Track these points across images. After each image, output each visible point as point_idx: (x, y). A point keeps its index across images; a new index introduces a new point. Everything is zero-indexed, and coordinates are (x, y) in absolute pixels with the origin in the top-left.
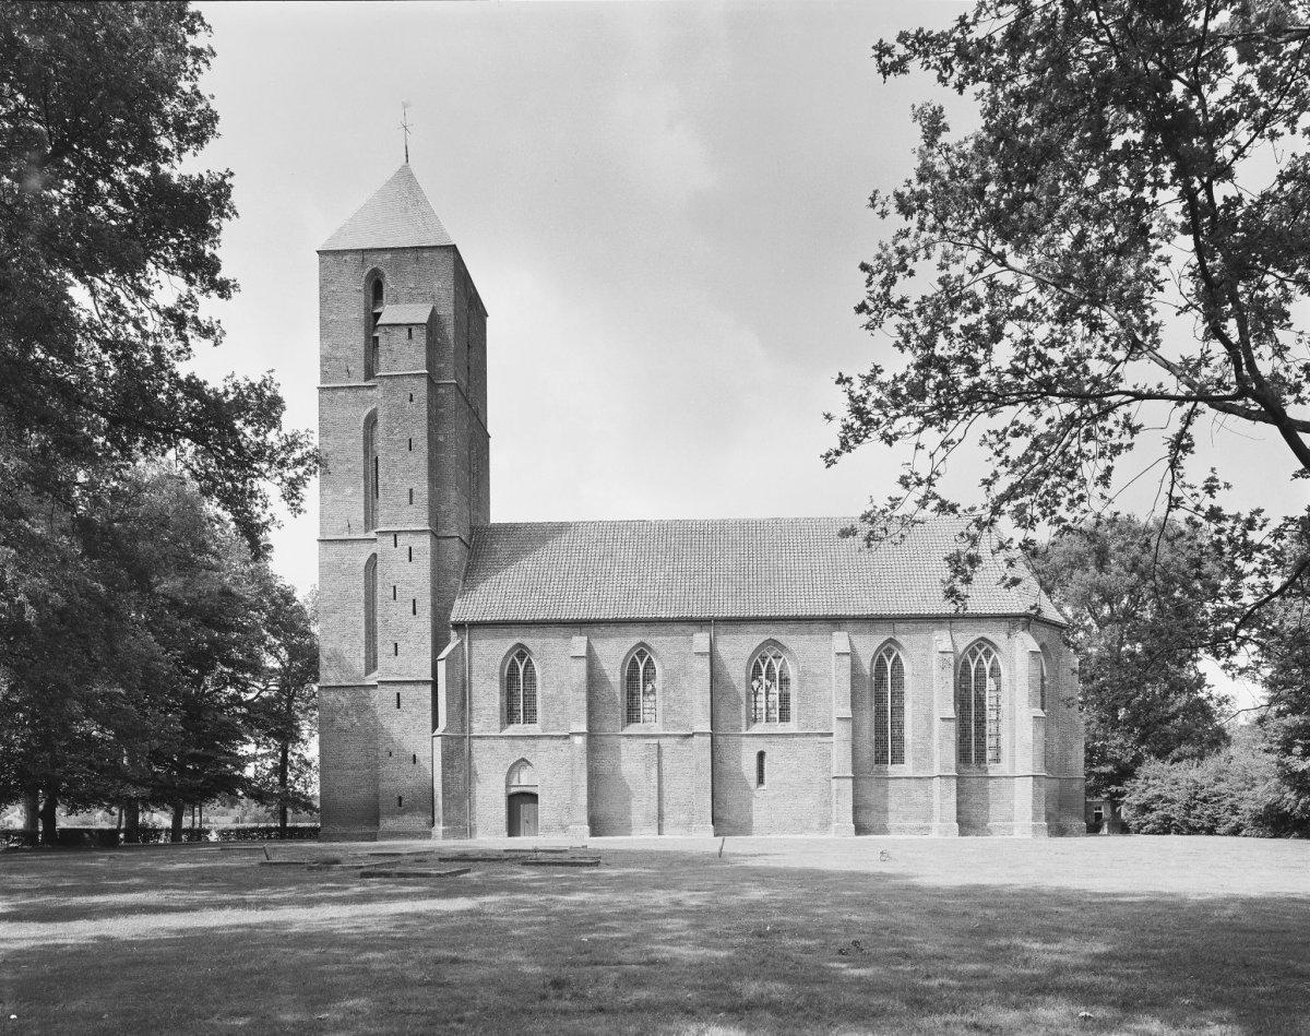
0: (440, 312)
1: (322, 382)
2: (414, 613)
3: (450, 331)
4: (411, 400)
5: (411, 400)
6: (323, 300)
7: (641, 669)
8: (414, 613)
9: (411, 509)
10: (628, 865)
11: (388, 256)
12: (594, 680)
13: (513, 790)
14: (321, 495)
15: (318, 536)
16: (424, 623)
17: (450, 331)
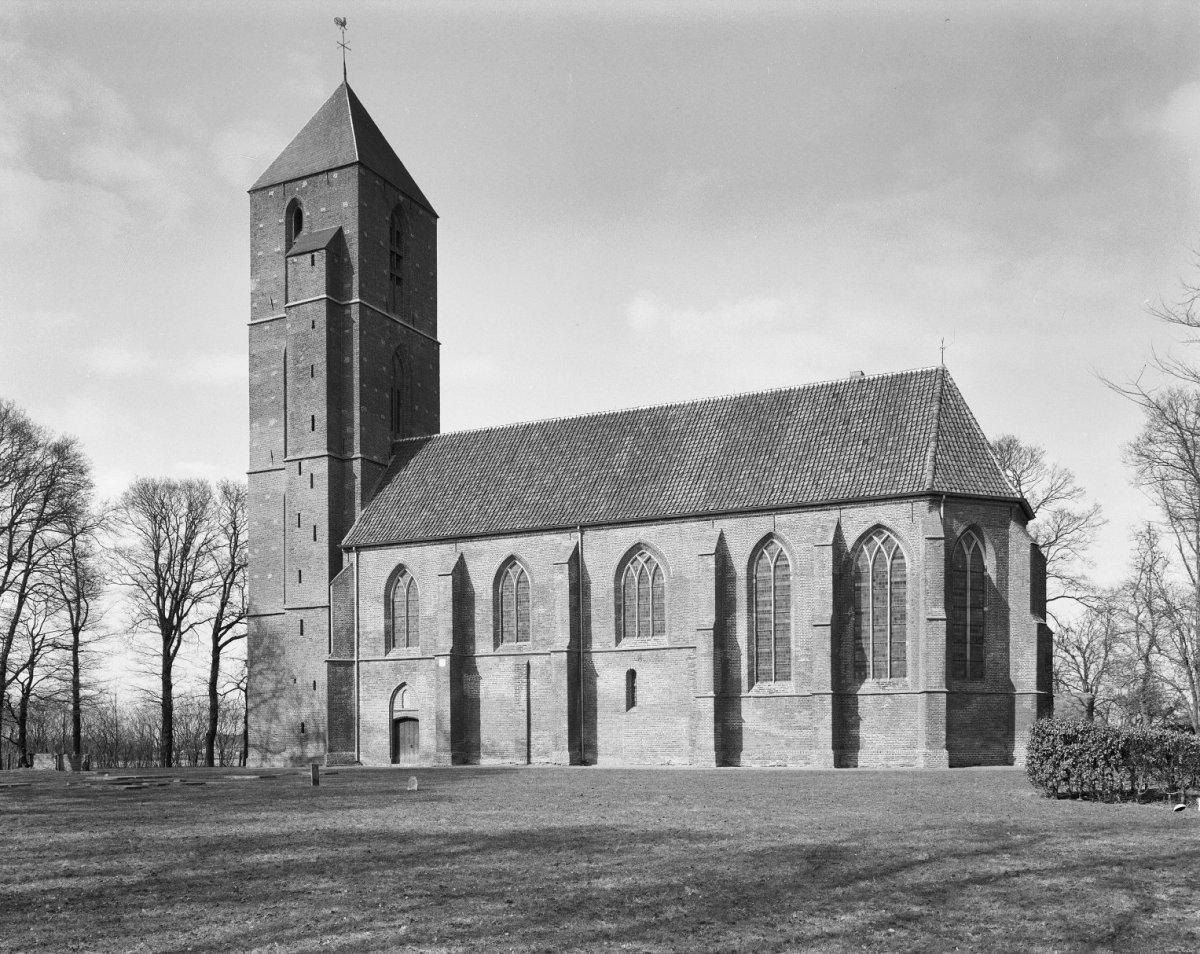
0: (347, 232)
1: (252, 319)
2: (315, 539)
3: (354, 251)
4: (313, 327)
5: (313, 327)
6: (254, 235)
7: (969, 558)
8: (315, 539)
9: (313, 435)
10: (750, 657)
11: (305, 183)
12: (579, 588)
13: (396, 716)
14: (251, 428)
15: (248, 469)
16: (322, 548)
17: (354, 251)
